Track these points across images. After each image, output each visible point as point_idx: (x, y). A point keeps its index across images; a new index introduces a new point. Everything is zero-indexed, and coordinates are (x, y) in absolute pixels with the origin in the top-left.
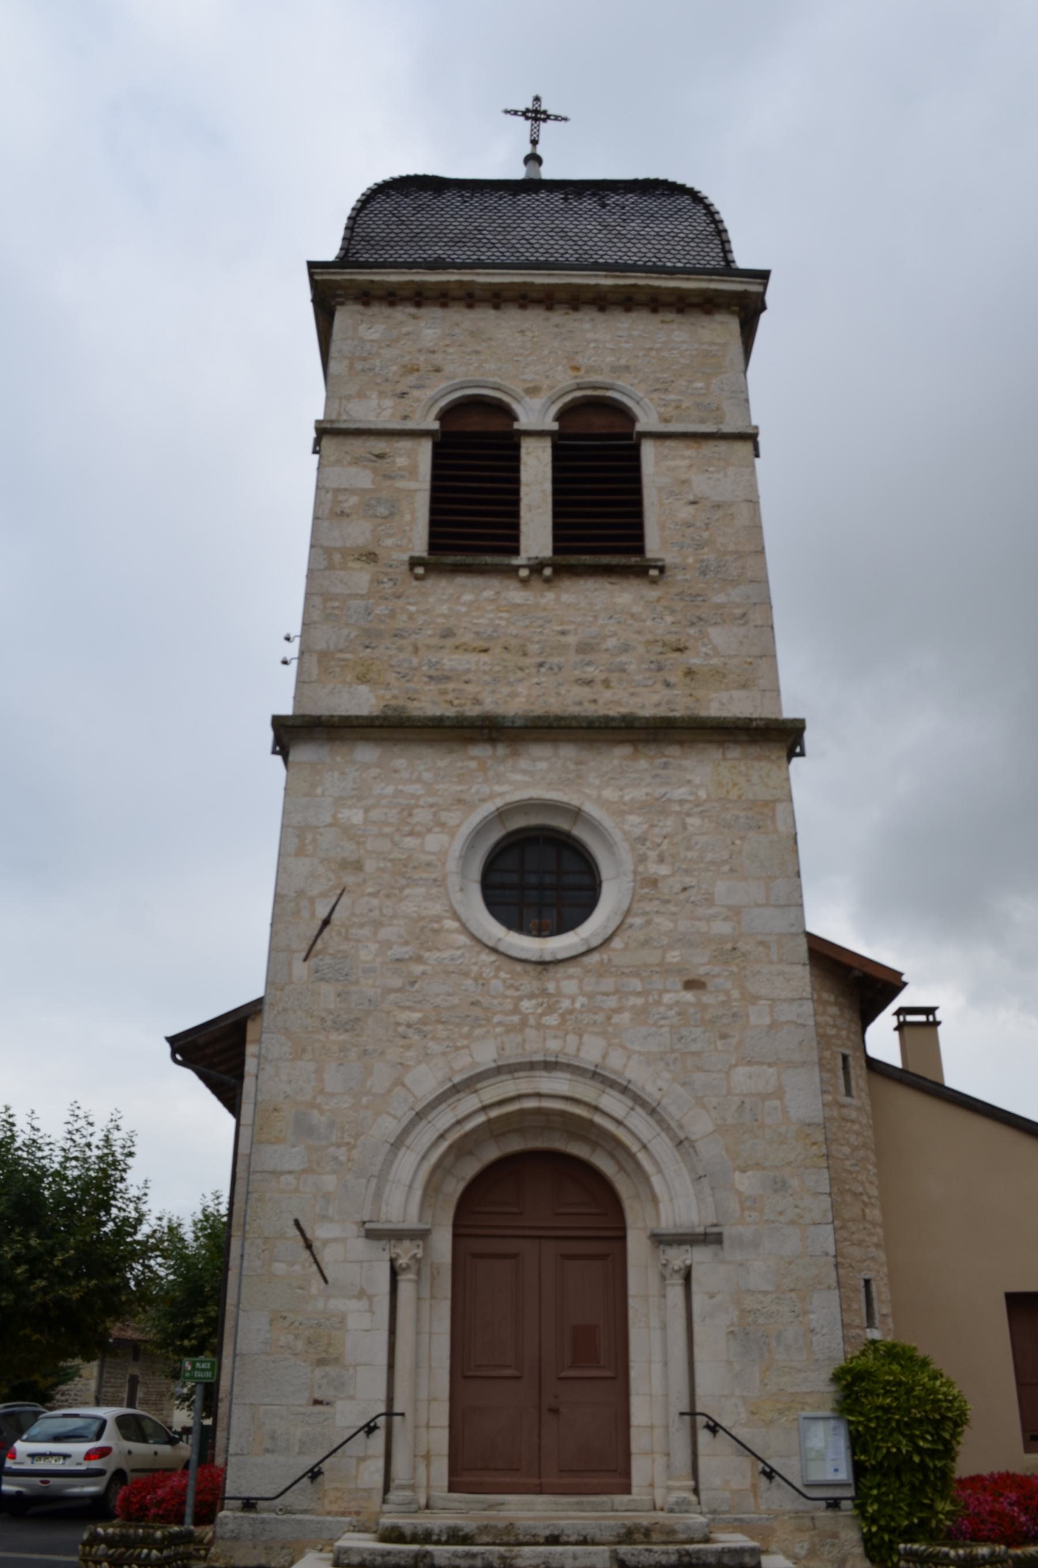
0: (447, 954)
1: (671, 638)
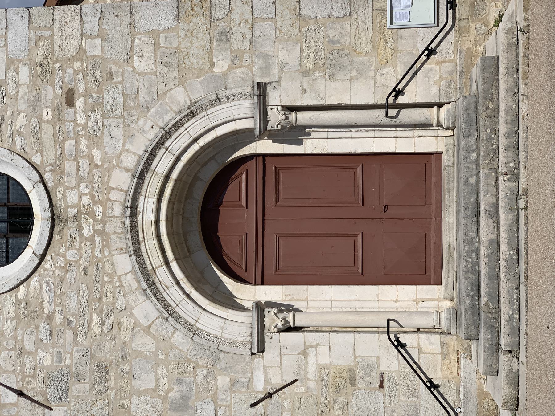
0: (46, 296)
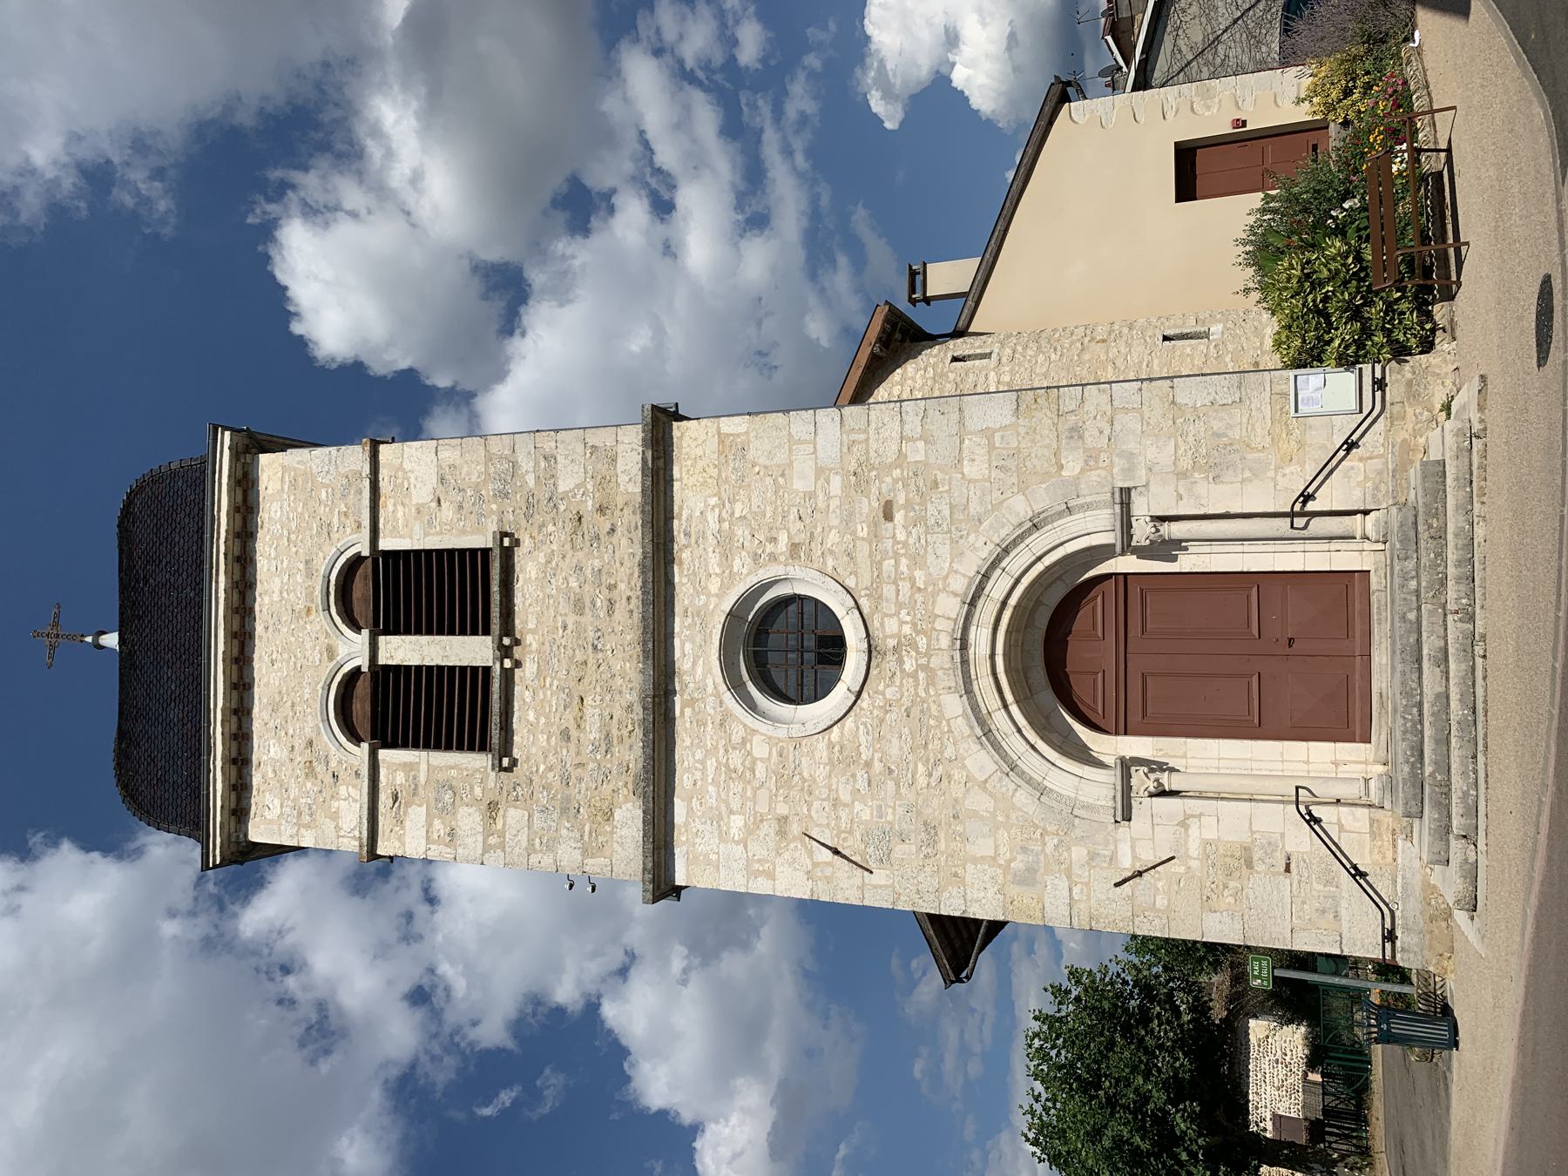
0: (863, 739)
1: (569, 527)
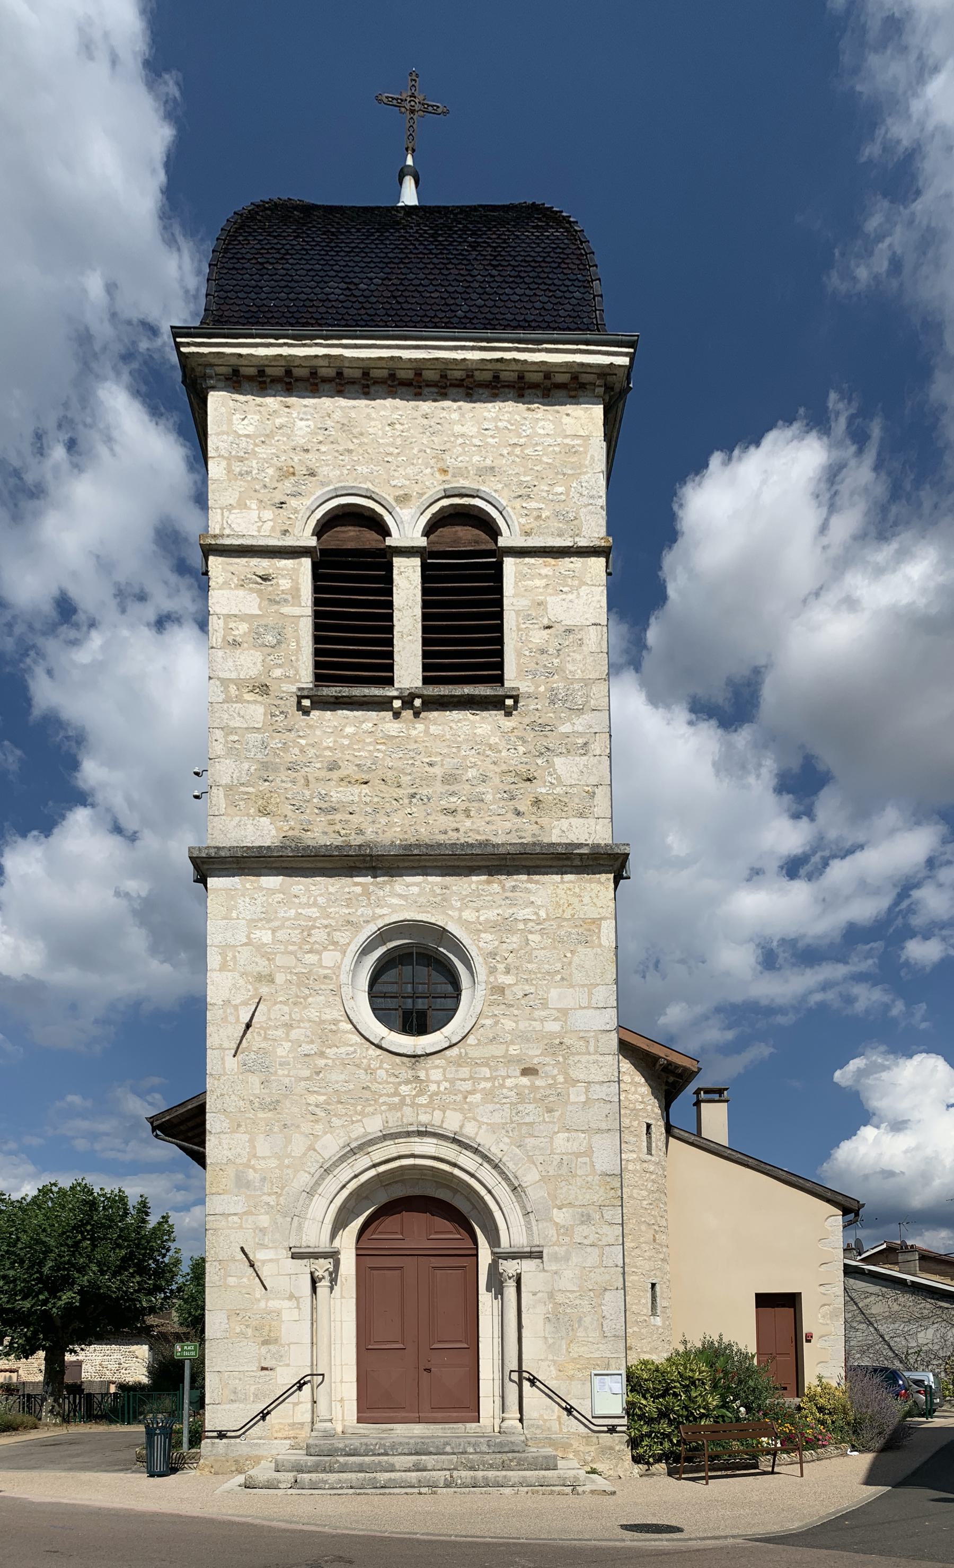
0: (343, 1050)
1: (522, 768)
